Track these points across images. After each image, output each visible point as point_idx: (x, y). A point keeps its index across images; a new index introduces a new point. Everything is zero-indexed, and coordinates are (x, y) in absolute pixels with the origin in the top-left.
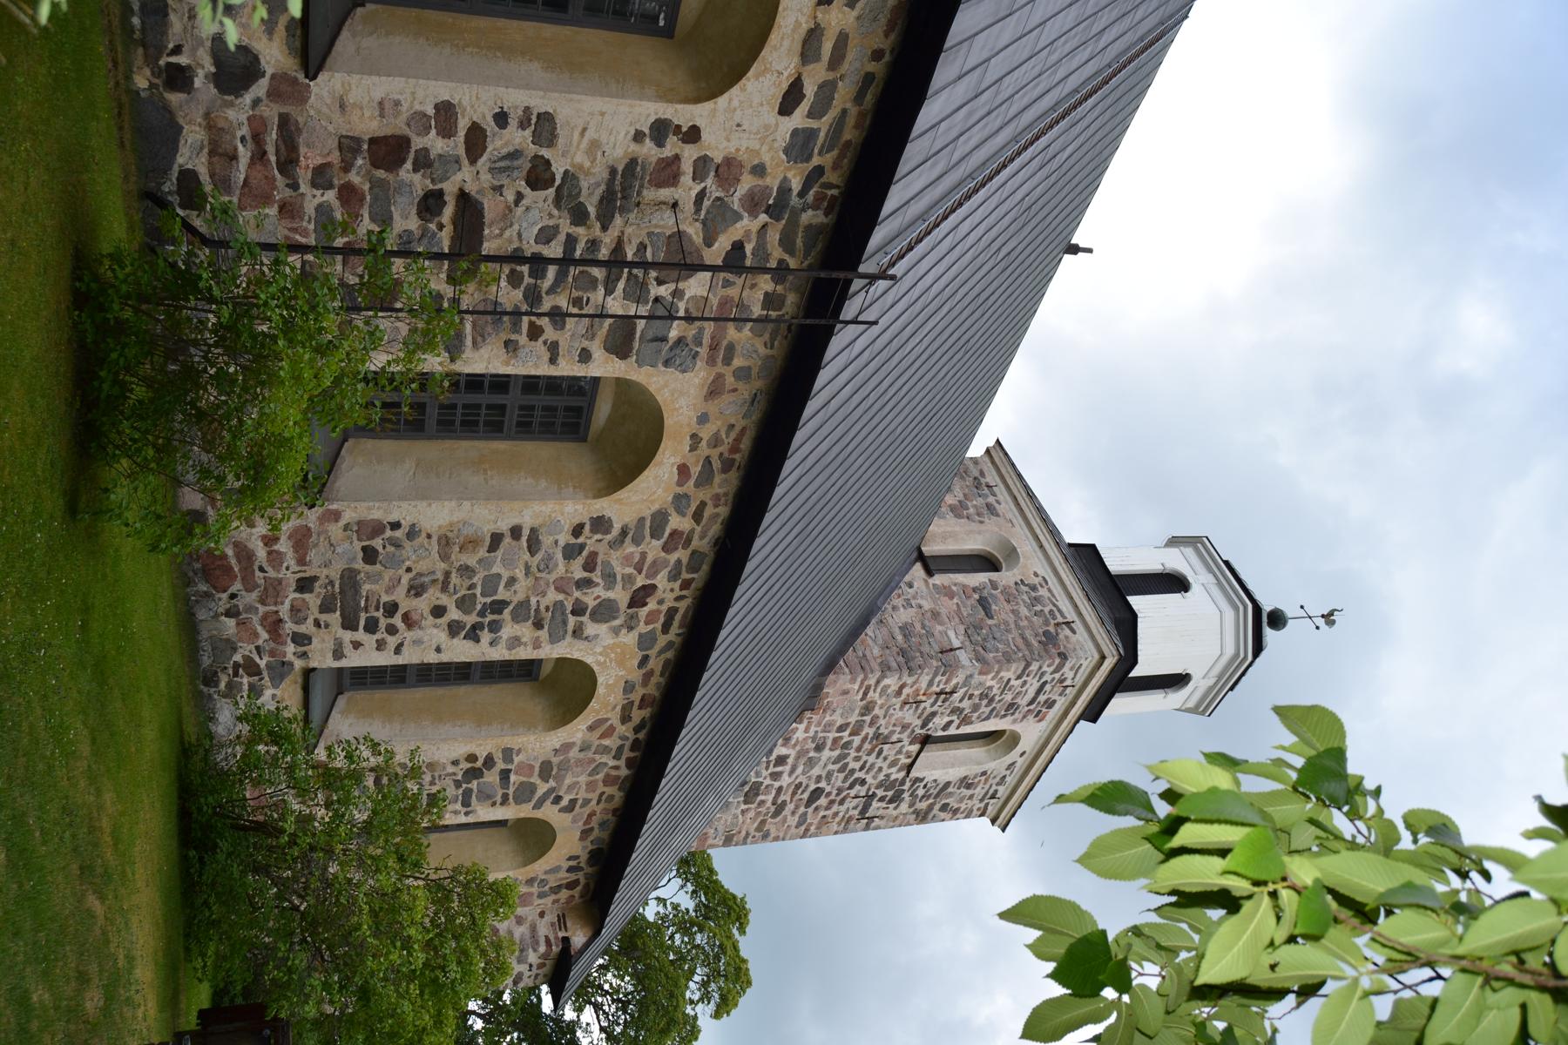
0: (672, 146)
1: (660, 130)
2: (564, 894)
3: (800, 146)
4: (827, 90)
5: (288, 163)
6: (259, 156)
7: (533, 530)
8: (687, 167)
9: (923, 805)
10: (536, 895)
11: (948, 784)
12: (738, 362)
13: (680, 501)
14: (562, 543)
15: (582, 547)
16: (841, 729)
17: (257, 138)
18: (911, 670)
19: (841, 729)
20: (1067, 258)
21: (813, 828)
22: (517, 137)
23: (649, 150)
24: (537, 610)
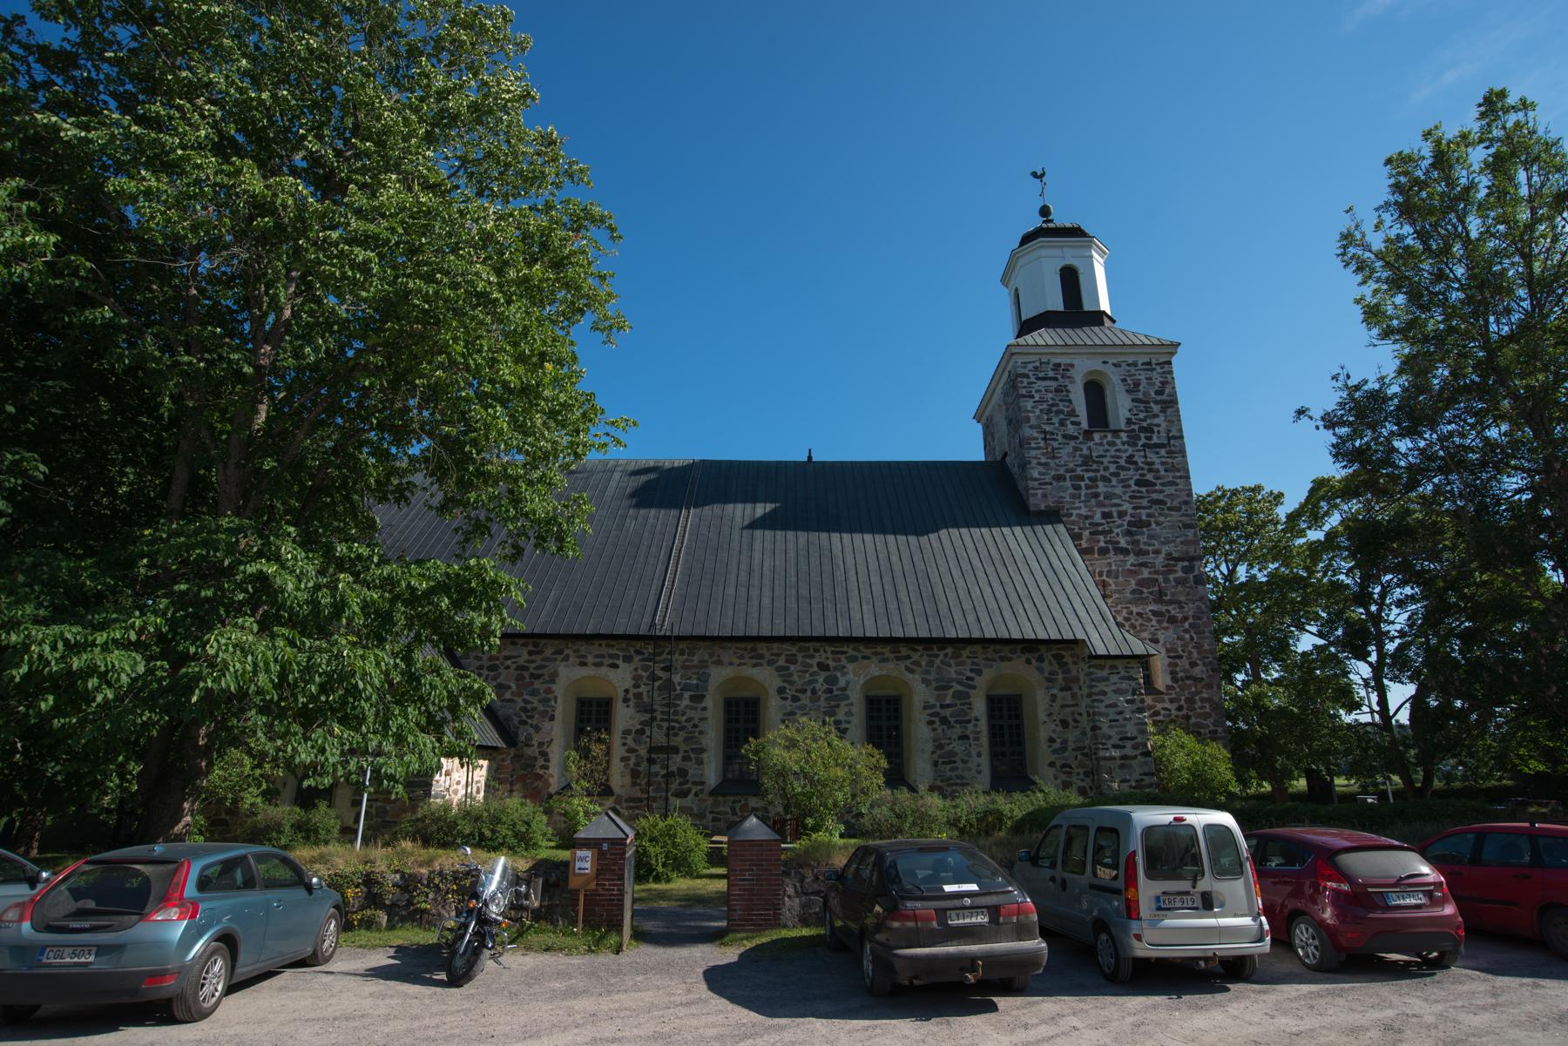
0: (630, 696)
1: (626, 700)
3: (628, 659)
4: (611, 656)
5: (640, 800)
6: (637, 808)
8: (636, 691)
9: (1156, 408)
12: (706, 657)
13: (770, 663)
15: (793, 696)
16: (1078, 488)
17: (632, 808)
19: (1078, 488)
22: (630, 740)
23: (631, 703)
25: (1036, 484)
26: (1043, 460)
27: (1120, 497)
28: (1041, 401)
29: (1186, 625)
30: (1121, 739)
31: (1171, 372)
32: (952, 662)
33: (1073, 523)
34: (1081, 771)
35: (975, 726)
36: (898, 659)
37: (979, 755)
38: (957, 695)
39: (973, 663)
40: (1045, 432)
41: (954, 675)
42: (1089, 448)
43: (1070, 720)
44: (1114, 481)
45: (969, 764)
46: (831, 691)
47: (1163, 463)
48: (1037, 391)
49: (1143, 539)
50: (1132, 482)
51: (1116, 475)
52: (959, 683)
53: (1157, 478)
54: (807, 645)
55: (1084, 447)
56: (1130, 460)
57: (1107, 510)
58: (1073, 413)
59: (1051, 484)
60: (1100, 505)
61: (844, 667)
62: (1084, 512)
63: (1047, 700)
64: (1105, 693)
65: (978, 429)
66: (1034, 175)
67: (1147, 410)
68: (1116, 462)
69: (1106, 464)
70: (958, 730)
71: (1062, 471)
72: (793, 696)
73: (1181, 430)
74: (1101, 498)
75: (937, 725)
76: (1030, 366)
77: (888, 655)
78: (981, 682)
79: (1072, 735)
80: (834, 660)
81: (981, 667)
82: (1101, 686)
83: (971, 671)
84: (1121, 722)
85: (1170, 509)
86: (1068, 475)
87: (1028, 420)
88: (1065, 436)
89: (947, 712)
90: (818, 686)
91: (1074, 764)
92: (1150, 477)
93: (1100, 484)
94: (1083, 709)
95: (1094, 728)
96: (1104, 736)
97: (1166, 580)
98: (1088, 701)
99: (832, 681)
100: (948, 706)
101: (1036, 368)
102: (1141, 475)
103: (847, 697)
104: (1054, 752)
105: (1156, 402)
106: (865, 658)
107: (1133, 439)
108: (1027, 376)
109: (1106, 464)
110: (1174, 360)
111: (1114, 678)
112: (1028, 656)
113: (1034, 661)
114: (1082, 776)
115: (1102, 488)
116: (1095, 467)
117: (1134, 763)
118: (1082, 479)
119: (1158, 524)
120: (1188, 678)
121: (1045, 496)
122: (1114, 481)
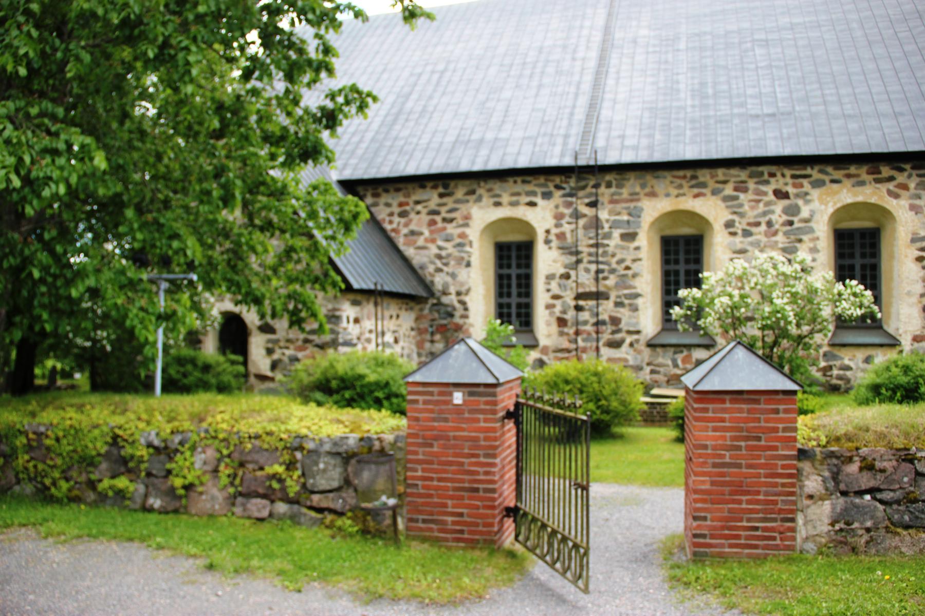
7: (735, 252)
14: (742, 239)
15: (744, 230)
36: (877, 181)
46: (791, 223)
54: (761, 169)
61: (807, 194)
72: (744, 230)
77: (865, 177)
90: (774, 217)
99: (793, 211)
103: (811, 230)
106: (834, 181)
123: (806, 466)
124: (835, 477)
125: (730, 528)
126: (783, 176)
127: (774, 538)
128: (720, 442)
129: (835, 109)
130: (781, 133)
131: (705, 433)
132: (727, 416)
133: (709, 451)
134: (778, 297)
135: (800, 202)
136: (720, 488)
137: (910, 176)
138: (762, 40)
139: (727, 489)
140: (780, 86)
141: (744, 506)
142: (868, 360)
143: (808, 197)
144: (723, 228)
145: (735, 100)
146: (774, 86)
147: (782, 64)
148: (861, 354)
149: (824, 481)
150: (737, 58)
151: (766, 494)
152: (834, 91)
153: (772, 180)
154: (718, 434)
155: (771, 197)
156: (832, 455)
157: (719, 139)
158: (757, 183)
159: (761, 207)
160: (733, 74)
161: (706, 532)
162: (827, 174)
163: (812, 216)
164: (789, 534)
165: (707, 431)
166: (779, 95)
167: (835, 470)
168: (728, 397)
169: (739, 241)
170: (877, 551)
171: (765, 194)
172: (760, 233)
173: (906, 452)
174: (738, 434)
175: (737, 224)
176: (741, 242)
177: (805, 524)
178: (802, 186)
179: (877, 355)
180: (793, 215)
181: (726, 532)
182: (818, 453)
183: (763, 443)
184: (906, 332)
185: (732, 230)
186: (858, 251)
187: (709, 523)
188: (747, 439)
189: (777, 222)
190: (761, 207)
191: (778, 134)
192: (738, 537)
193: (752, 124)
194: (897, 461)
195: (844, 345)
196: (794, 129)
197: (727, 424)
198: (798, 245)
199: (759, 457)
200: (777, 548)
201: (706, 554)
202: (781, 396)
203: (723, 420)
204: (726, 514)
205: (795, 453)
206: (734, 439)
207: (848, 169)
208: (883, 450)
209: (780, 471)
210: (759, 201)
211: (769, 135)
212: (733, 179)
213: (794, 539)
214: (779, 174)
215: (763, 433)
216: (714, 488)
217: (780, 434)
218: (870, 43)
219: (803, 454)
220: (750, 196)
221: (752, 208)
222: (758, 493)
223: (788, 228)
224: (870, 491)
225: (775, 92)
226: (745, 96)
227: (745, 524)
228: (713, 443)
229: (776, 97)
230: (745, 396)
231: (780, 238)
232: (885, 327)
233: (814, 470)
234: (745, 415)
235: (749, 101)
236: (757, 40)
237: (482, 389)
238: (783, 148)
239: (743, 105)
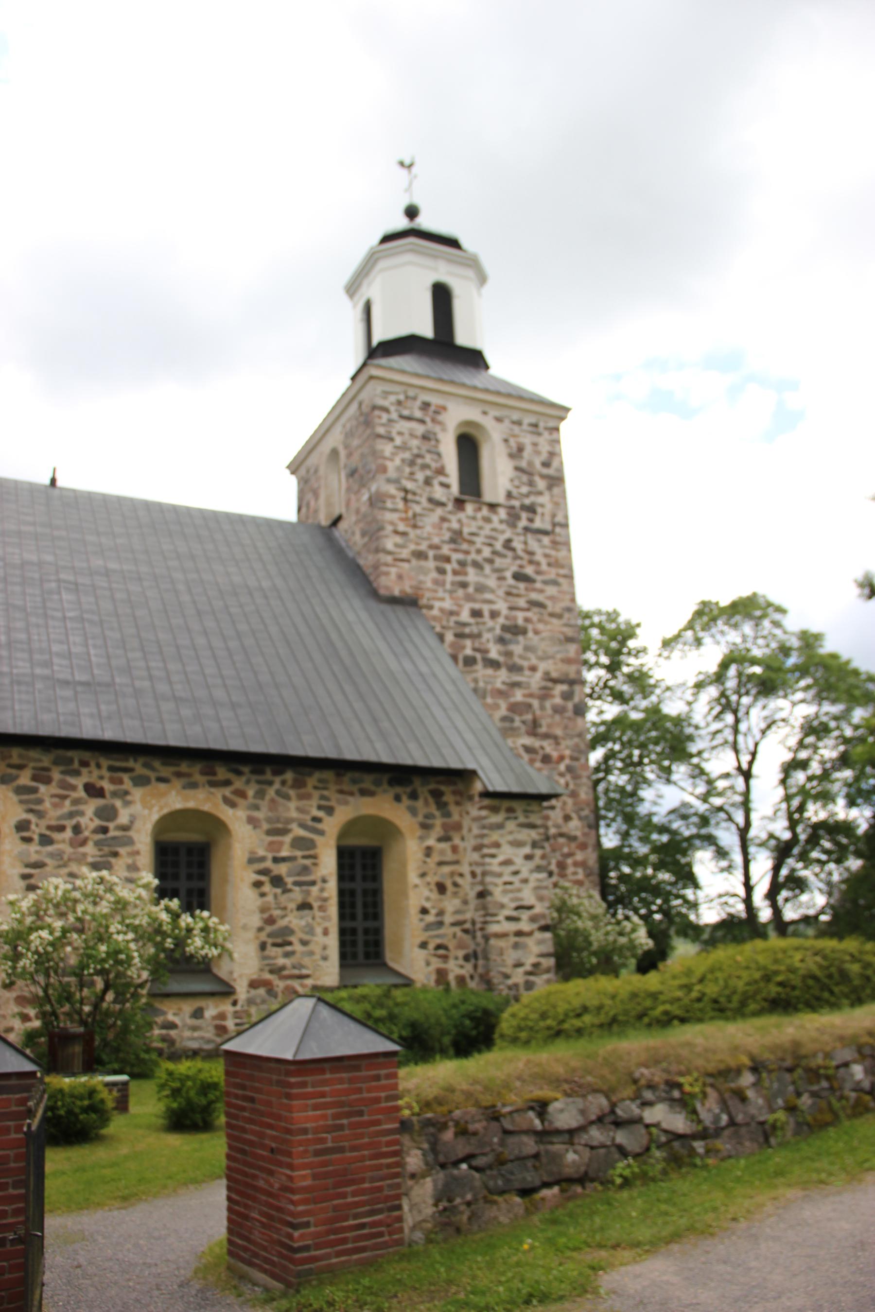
2: (448, 798)
7: (28, 866)
9: (541, 484)
10: (446, 820)
11: (518, 469)
14: (38, 848)
15: (42, 836)
16: (442, 571)
18: (382, 528)
19: (442, 571)
20: (60, 483)
21: (562, 572)
24: (101, 856)
25: (389, 559)
26: (402, 527)
27: (492, 591)
28: (404, 447)
29: (562, 767)
30: (518, 908)
31: (558, 442)
32: (292, 793)
33: (435, 618)
34: (461, 953)
35: (322, 890)
36: (213, 784)
37: (326, 932)
38: (298, 843)
39: (323, 797)
40: (406, 491)
41: (294, 814)
42: (459, 521)
43: (448, 884)
44: (487, 568)
45: (311, 947)
46: (104, 830)
47: (546, 556)
48: (400, 433)
49: (517, 649)
50: (508, 574)
51: (490, 561)
52: (303, 826)
53: (538, 573)
54: (70, 754)
55: (453, 518)
56: (508, 545)
57: (477, 606)
58: (441, 471)
59: (408, 561)
60: (469, 598)
61: (127, 793)
62: (448, 604)
63: (420, 855)
64: (497, 845)
65: (291, 484)
66: (402, 164)
67: (531, 484)
68: (490, 545)
69: (478, 545)
70: (297, 895)
71: (423, 547)
72: (42, 836)
73: (566, 517)
74: (471, 590)
75: (267, 888)
76: (393, 398)
77: (198, 778)
78: (332, 825)
79: (451, 904)
80: (112, 781)
81: (332, 803)
82: (495, 836)
83: (320, 808)
84: (517, 884)
85: (552, 615)
86: (431, 553)
87: (384, 470)
88: (431, 500)
89: (282, 869)
90: (83, 821)
91: (451, 945)
92: (529, 570)
93: (471, 570)
94: (465, 869)
95: (482, 895)
96: (496, 903)
97: (542, 708)
98: (476, 856)
99: (107, 814)
100: (284, 860)
101: (399, 403)
102: (521, 567)
103: (130, 842)
104: (428, 927)
105: (543, 477)
106: (161, 780)
107: (513, 518)
108: (386, 410)
109: (478, 545)
110: (563, 426)
111: (511, 825)
112: (398, 790)
113: (404, 798)
114: (461, 962)
115: (472, 576)
116: (465, 546)
117: (530, 942)
118: (448, 560)
119: (536, 632)
120: (561, 835)
121: (400, 577)
122: (487, 568)
123: (406, 1140)
124: (434, 1148)
125: (336, 1231)
126: (99, 766)
127: (381, 1234)
128: (321, 1123)
129: (163, 688)
130: (99, 711)
131: (305, 1114)
132: (327, 1089)
133: (310, 1136)
134: (118, 933)
135: (118, 803)
136: (323, 1181)
137: (248, 782)
138: (69, 582)
139: (330, 1181)
140: (95, 646)
141: (350, 1199)
142: (198, 1014)
143: (129, 798)
144: (14, 830)
145: (37, 657)
146: (87, 646)
147: (96, 618)
148: (188, 1007)
149: (424, 1155)
150: (38, 599)
151: (373, 1180)
152: (161, 665)
153: (84, 770)
154: (318, 1112)
155: (81, 793)
156: (429, 1123)
157: (17, 707)
158: (63, 772)
159: (67, 806)
160: (33, 620)
161: (310, 1242)
162: (153, 769)
163: (132, 822)
164: (397, 1225)
165: (307, 1111)
166: (93, 659)
167: (432, 1139)
168: (326, 1066)
169: (34, 851)
170: (480, 1226)
171: (74, 788)
172: (63, 841)
173: (493, 1110)
174: (339, 1110)
175: (33, 827)
176: (37, 852)
177: (411, 1210)
178: (121, 782)
179: (208, 1007)
180: (109, 819)
181: (332, 1237)
182: (415, 1122)
183: (366, 1118)
184: (241, 976)
185: (25, 834)
186: (183, 872)
187: (312, 1229)
188: (349, 1115)
189: (87, 828)
190: (67, 806)
191: (95, 711)
192: (344, 1241)
193: (60, 692)
194: (486, 1120)
195: (168, 995)
196: (114, 707)
197: (328, 1099)
198: (113, 860)
199: (362, 1136)
200: (385, 1245)
201: (310, 1272)
202: (381, 1060)
203: (323, 1095)
204: (330, 1214)
205: (397, 1125)
206: (336, 1116)
207: (178, 765)
208: (473, 1110)
209: (385, 1149)
210: (64, 797)
211: (84, 710)
212: (32, 764)
213: (401, 1230)
214: (93, 764)
215: (365, 1106)
216: (317, 1182)
217: (383, 1105)
218: (199, 613)
219: (405, 1126)
220: (54, 789)
221: (55, 806)
222: (363, 1181)
223: (101, 836)
224: (467, 1158)
225: (88, 654)
226: (50, 652)
227: (352, 1222)
228: (314, 1125)
229: (90, 661)
230: (346, 1063)
231: (90, 849)
232: (215, 970)
233: (414, 1144)
234: (346, 1086)
235: (56, 660)
236: (65, 581)
237: (13, 1082)
238: (103, 730)
239: (48, 664)
